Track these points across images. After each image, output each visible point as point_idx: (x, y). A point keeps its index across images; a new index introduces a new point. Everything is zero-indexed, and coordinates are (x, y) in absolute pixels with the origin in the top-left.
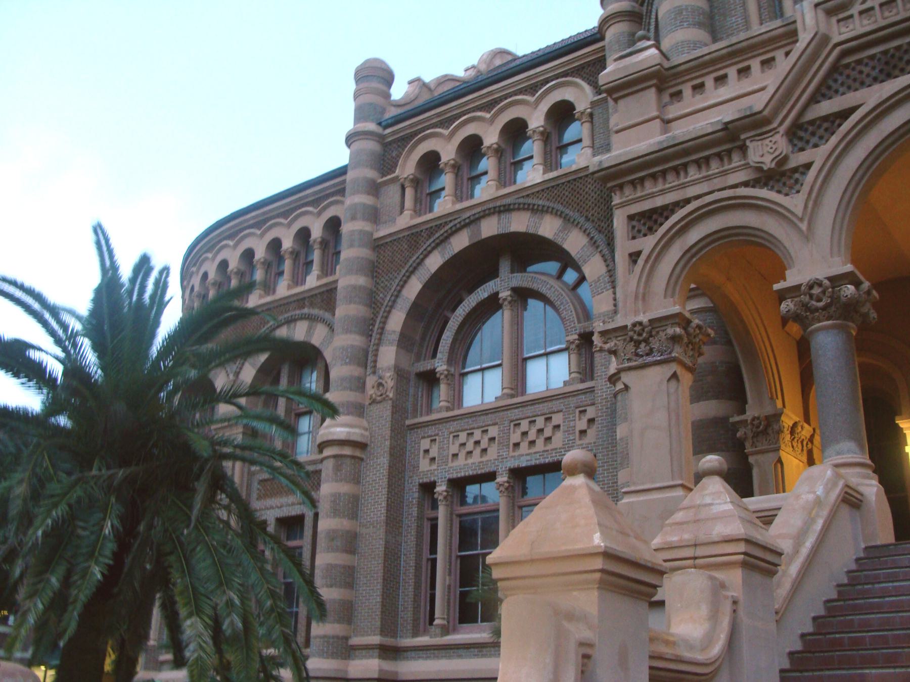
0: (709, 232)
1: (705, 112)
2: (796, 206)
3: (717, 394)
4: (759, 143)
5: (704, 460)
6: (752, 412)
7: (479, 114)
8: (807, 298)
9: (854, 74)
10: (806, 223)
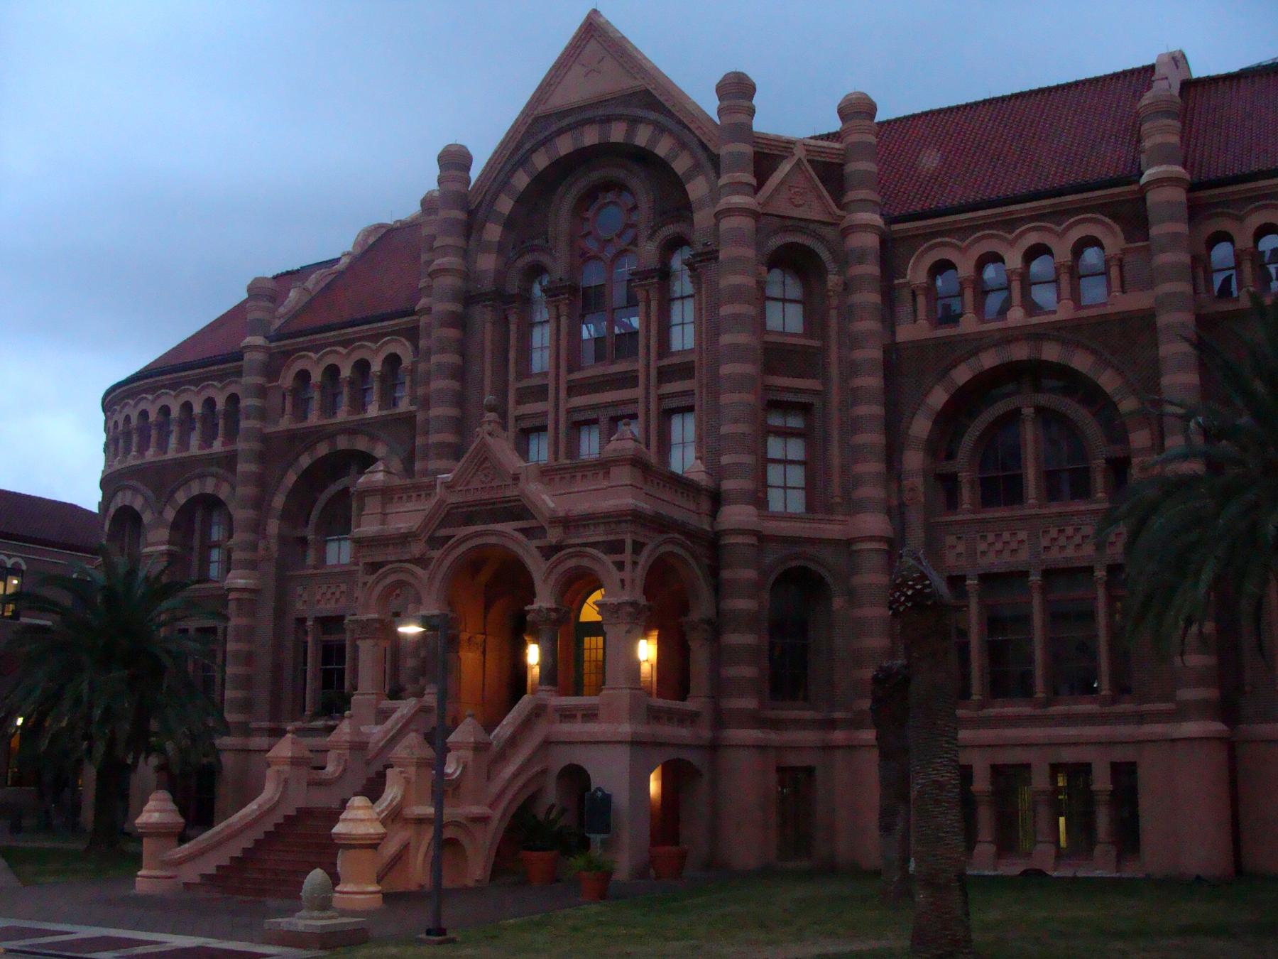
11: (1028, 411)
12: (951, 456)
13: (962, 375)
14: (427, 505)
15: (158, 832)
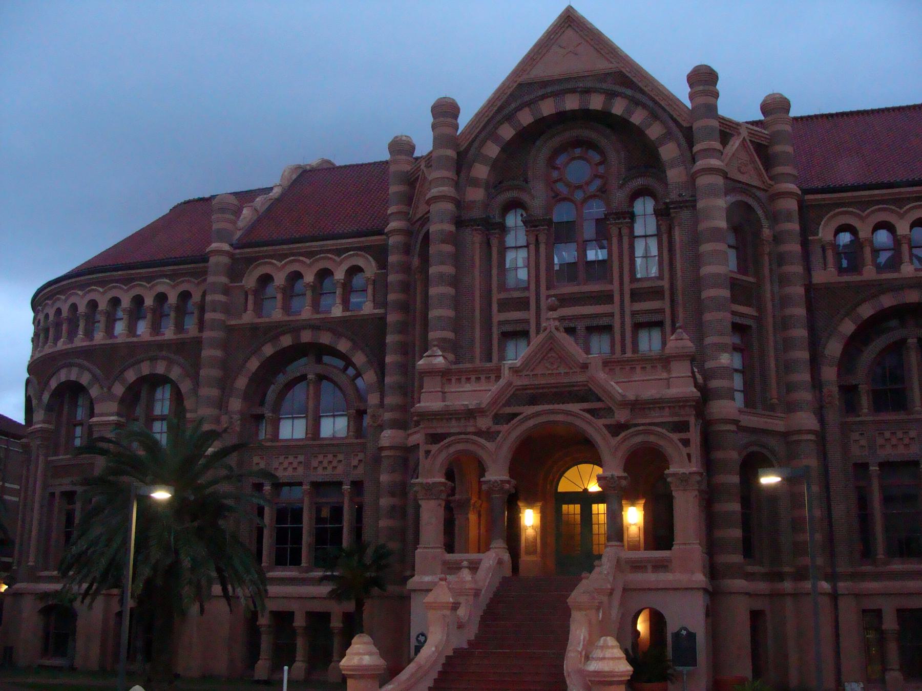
7: (301, 258)
11: (912, 341)
12: (262, 404)
13: (866, 311)
14: (495, 387)
15: (362, 673)
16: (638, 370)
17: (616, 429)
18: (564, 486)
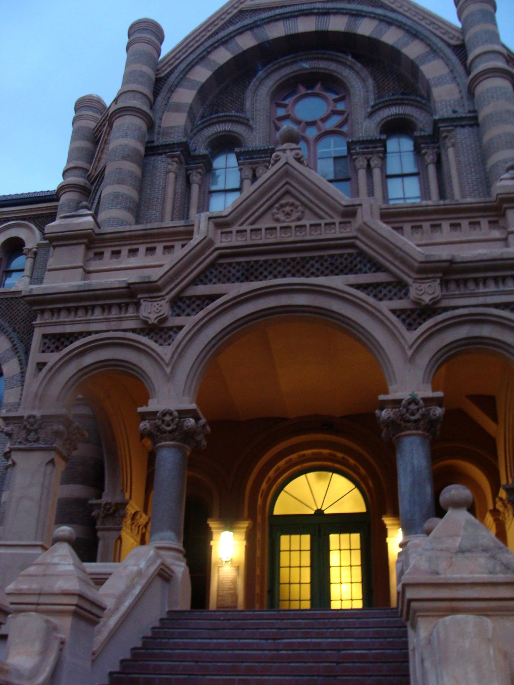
0: (98, 360)
1: (116, 272)
2: (166, 354)
3: (84, 482)
4: (150, 303)
5: (59, 529)
6: (106, 499)
8: (160, 422)
9: (225, 272)
10: (170, 367)
16: (445, 225)
17: (415, 315)
18: (283, 506)
